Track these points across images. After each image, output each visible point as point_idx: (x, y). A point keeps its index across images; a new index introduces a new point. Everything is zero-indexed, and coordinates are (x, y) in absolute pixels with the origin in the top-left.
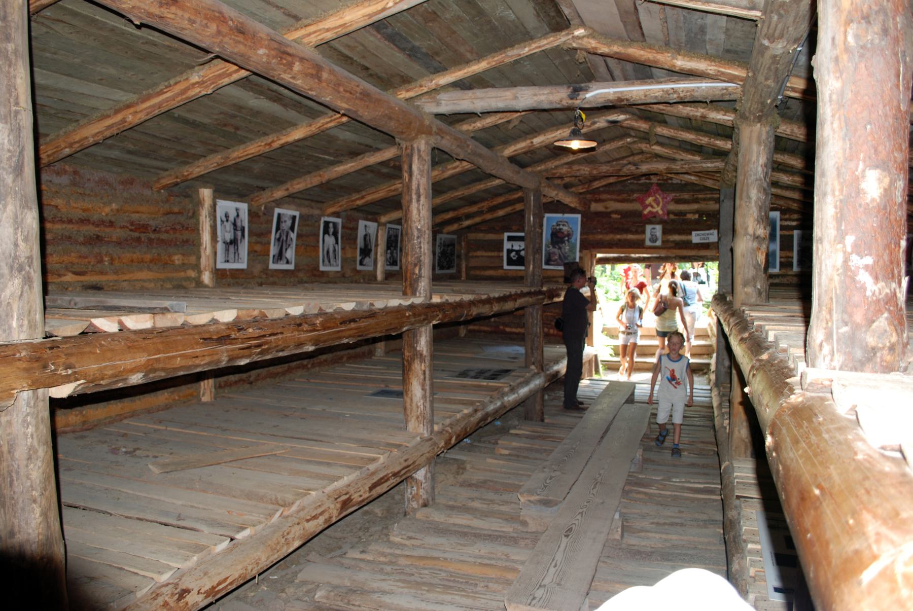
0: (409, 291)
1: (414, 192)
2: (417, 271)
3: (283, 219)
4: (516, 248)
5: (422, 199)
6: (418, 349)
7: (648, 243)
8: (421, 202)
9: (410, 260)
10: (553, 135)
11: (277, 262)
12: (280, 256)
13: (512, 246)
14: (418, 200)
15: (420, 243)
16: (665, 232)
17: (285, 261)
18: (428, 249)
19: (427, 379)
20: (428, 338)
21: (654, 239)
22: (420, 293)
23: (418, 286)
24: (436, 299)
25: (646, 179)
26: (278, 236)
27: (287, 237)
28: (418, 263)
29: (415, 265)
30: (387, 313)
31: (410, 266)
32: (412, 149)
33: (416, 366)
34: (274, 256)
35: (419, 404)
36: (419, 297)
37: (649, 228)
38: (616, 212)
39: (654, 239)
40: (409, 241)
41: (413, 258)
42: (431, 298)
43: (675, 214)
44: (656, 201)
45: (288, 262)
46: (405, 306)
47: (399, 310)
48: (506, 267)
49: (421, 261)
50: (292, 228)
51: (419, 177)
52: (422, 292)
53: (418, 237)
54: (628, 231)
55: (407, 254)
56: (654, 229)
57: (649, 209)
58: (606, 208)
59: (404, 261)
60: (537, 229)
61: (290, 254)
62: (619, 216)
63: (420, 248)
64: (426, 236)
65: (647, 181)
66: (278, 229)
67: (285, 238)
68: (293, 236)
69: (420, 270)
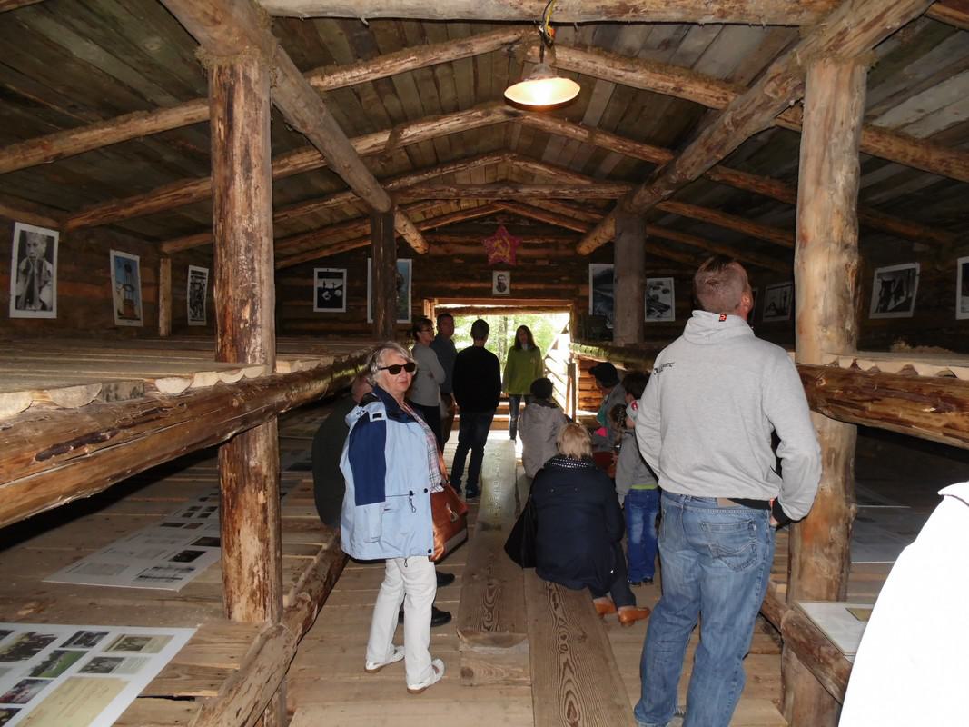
0: (229, 354)
1: (237, 160)
2: (246, 314)
3: (31, 240)
4: (329, 286)
5: (255, 173)
6: (252, 463)
7: (495, 291)
8: (253, 181)
9: (231, 293)
10: (430, 127)
11: (24, 308)
12: (29, 299)
13: (325, 284)
14: (247, 178)
15: (253, 260)
16: (513, 280)
17: (39, 306)
18: (267, 274)
19: (270, 519)
20: (271, 443)
21: (501, 287)
22: (254, 358)
23: (249, 344)
24: (283, 368)
25: (491, 220)
26: (23, 266)
27: (40, 270)
28: (250, 297)
29: (243, 303)
30: (191, 406)
31: (231, 305)
32: (234, 74)
33: (248, 497)
34: (18, 298)
35: (255, 569)
36: (253, 365)
37: (496, 274)
38: (459, 256)
39: (501, 287)
40: (229, 256)
41: (238, 291)
42: (274, 367)
43: (525, 259)
44: (504, 244)
45: (44, 307)
46: (230, 385)
47: (218, 397)
48: (316, 309)
49: (254, 295)
50: (48, 256)
51: (247, 131)
52: (257, 354)
53: (248, 250)
54: (471, 278)
55: (225, 284)
56: (502, 276)
57: (496, 253)
58: (448, 251)
59: (217, 295)
60: (390, 266)
61: (49, 294)
62: (462, 262)
63: (253, 270)
64: (264, 248)
65: (493, 223)
66: (22, 255)
67: (36, 271)
68: (52, 268)
69: (253, 312)
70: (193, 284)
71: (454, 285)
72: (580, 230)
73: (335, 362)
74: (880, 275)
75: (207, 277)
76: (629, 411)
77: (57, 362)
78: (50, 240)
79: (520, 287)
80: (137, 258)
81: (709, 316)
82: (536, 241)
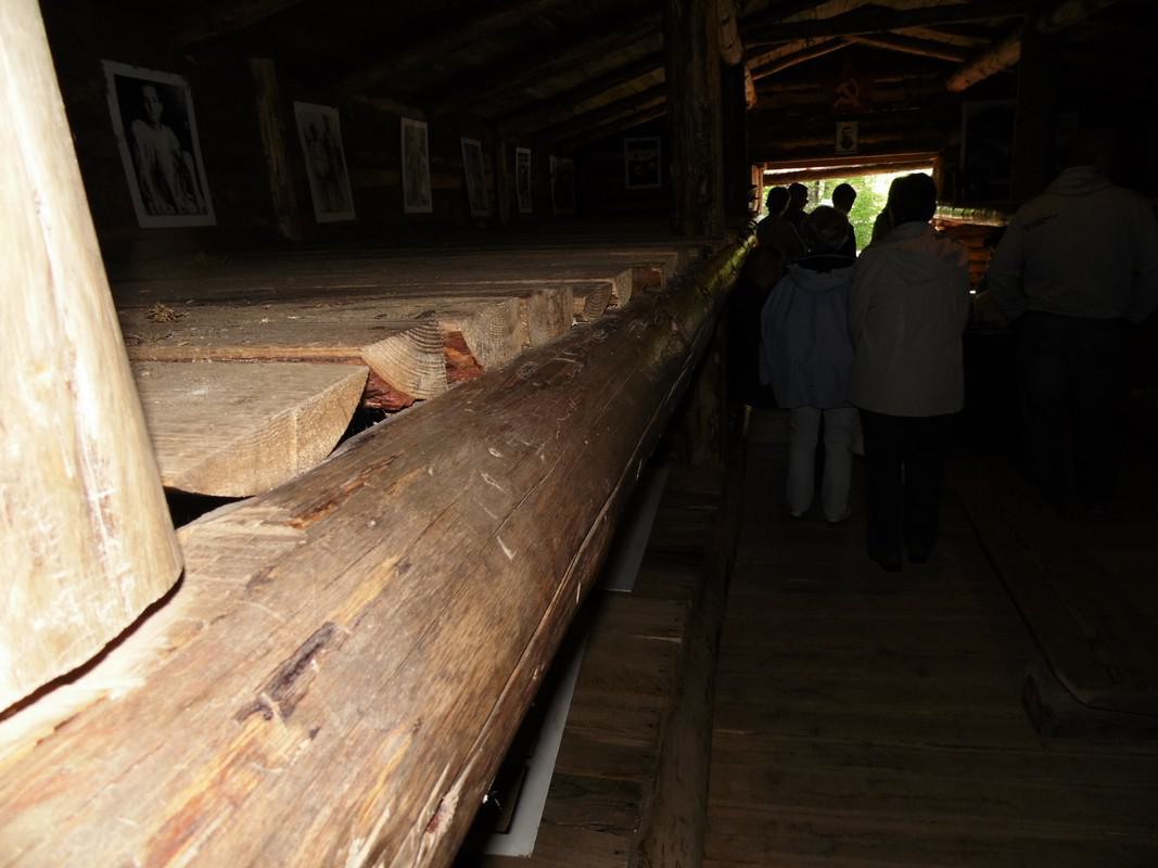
7: (839, 147)
16: (862, 132)
21: (846, 143)
39: (846, 143)
70: (520, 168)
71: (788, 146)
72: (956, 60)
73: (637, 285)
74: (768, 180)
75: (529, 158)
76: (508, 482)
77: (113, 332)
78: (423, 130)
79: (870, 141)
80: (478, 144)
81: (65, 357)
82: (893, 80)
